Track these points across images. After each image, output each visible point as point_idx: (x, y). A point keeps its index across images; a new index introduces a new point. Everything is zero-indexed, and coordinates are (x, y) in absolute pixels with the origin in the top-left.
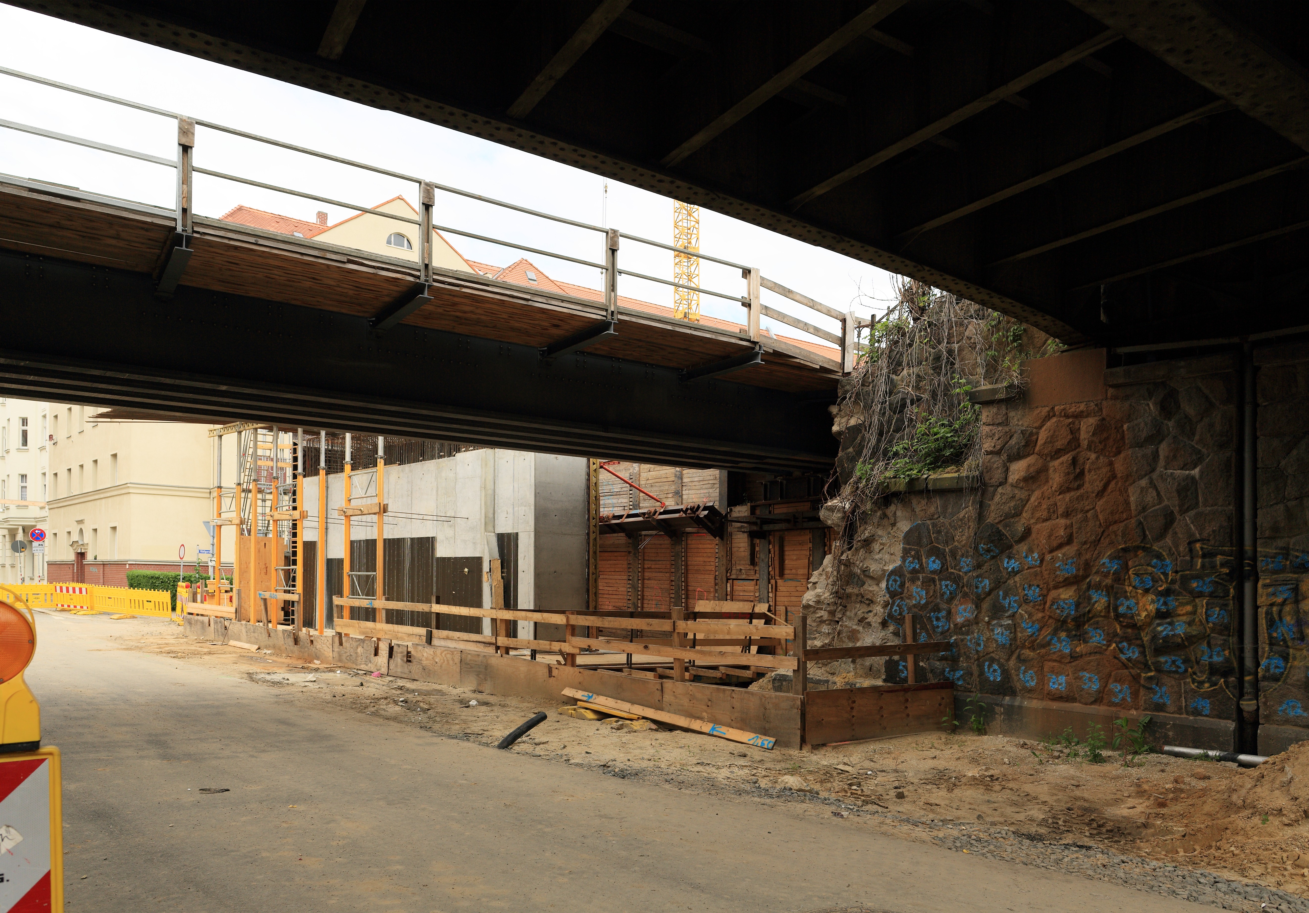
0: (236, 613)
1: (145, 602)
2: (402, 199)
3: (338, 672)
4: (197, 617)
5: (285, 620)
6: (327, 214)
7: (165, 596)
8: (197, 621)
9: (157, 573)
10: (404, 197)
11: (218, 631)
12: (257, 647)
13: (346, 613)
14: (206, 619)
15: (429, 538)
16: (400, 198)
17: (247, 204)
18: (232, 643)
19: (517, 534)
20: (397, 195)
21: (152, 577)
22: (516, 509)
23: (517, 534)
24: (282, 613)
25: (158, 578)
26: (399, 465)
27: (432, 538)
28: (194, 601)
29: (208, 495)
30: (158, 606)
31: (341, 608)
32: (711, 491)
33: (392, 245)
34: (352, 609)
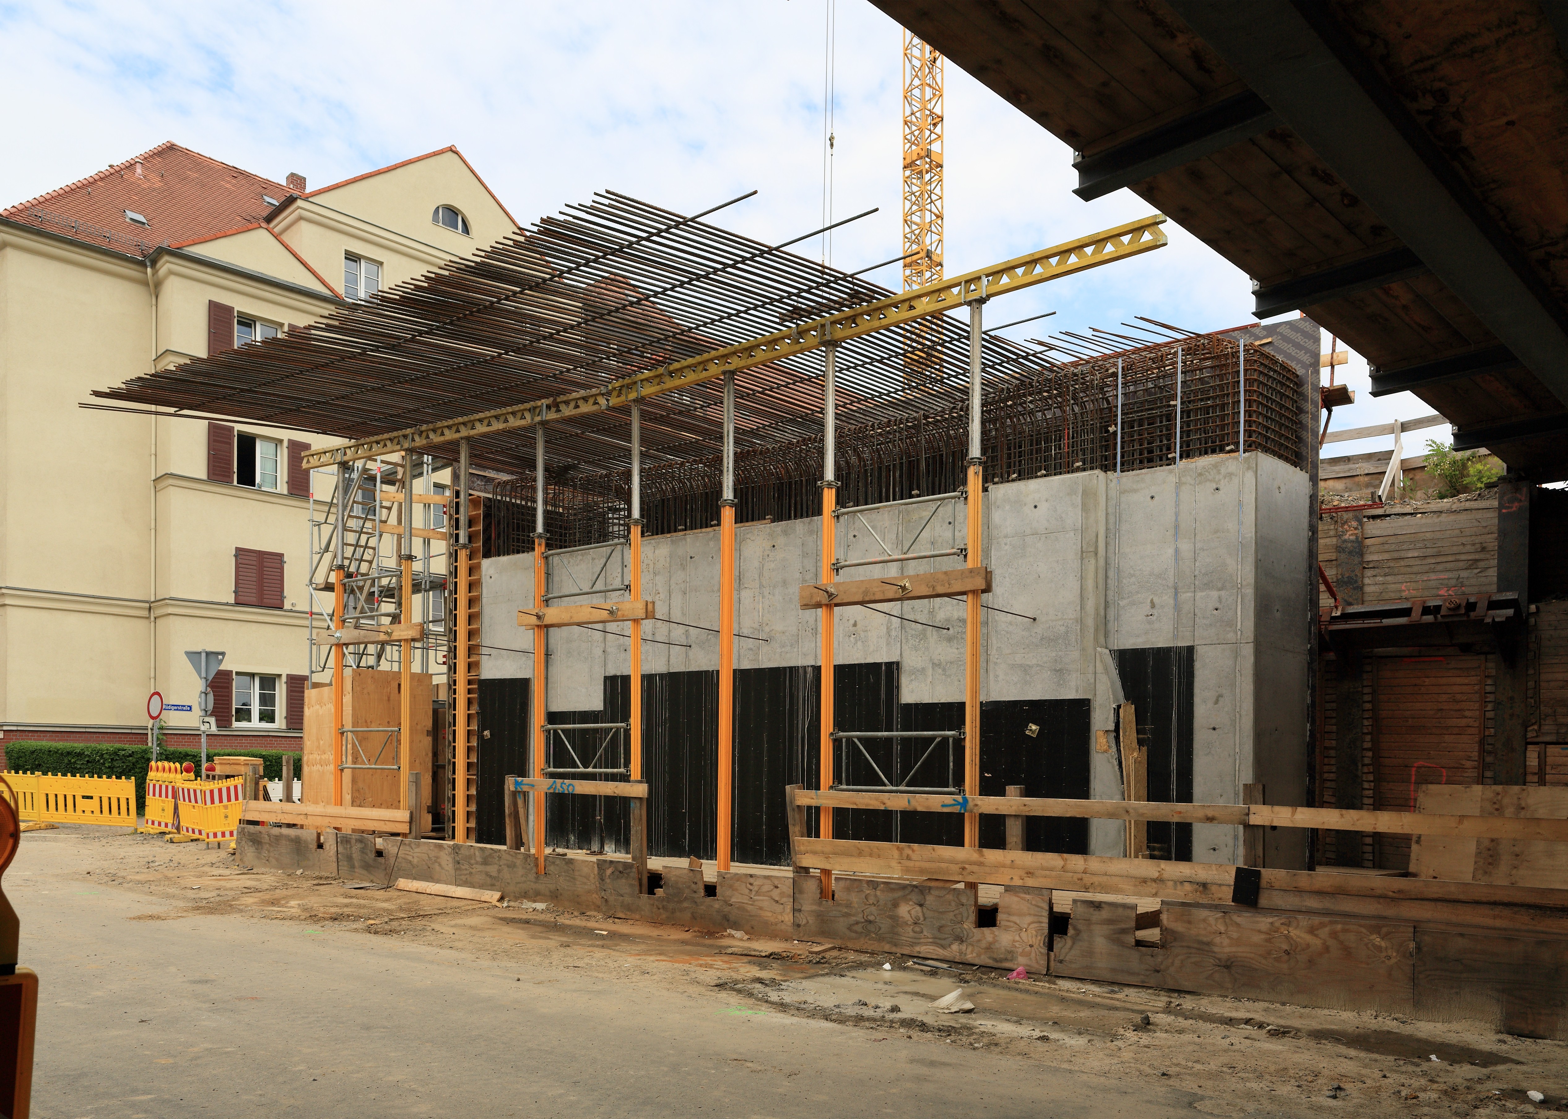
0: (411, 822)
1: (79, 800)
2: (456, 153)
3: (887, 966)
4: (276, 831)
5: (433, 830)
6: (305, 179)
7: (125, 788)
8: (278, 838)
9: (78, 745)
10: (459, 149)
11: (350, 858)
12: (497, 895)
13: (826, 824)
14: (308, 835)
15: (876, 666)
16: (452, 150)
17: (182, 142)
18: (402, 883)
19: (1190, 650)
20: (448, 145)
21: (69, 753)
22: (1186, 596)
23: (1190, 650)
24: (429, 817)
25: (80, 755)
26: (773, 521)
27: (889, 665)
28: (255, 799)
29: (145, 613)
30: (108, 806)
31: (813, 813)
32: (1464, 574)
33: (441, 224)
34: (840, 814)
